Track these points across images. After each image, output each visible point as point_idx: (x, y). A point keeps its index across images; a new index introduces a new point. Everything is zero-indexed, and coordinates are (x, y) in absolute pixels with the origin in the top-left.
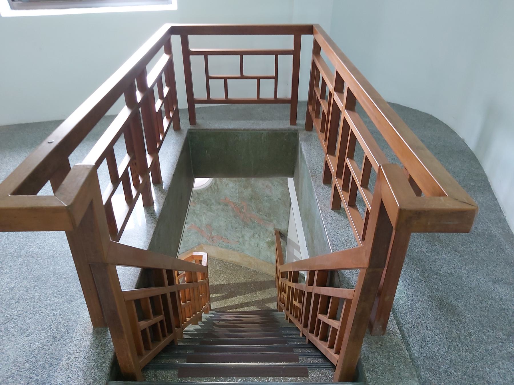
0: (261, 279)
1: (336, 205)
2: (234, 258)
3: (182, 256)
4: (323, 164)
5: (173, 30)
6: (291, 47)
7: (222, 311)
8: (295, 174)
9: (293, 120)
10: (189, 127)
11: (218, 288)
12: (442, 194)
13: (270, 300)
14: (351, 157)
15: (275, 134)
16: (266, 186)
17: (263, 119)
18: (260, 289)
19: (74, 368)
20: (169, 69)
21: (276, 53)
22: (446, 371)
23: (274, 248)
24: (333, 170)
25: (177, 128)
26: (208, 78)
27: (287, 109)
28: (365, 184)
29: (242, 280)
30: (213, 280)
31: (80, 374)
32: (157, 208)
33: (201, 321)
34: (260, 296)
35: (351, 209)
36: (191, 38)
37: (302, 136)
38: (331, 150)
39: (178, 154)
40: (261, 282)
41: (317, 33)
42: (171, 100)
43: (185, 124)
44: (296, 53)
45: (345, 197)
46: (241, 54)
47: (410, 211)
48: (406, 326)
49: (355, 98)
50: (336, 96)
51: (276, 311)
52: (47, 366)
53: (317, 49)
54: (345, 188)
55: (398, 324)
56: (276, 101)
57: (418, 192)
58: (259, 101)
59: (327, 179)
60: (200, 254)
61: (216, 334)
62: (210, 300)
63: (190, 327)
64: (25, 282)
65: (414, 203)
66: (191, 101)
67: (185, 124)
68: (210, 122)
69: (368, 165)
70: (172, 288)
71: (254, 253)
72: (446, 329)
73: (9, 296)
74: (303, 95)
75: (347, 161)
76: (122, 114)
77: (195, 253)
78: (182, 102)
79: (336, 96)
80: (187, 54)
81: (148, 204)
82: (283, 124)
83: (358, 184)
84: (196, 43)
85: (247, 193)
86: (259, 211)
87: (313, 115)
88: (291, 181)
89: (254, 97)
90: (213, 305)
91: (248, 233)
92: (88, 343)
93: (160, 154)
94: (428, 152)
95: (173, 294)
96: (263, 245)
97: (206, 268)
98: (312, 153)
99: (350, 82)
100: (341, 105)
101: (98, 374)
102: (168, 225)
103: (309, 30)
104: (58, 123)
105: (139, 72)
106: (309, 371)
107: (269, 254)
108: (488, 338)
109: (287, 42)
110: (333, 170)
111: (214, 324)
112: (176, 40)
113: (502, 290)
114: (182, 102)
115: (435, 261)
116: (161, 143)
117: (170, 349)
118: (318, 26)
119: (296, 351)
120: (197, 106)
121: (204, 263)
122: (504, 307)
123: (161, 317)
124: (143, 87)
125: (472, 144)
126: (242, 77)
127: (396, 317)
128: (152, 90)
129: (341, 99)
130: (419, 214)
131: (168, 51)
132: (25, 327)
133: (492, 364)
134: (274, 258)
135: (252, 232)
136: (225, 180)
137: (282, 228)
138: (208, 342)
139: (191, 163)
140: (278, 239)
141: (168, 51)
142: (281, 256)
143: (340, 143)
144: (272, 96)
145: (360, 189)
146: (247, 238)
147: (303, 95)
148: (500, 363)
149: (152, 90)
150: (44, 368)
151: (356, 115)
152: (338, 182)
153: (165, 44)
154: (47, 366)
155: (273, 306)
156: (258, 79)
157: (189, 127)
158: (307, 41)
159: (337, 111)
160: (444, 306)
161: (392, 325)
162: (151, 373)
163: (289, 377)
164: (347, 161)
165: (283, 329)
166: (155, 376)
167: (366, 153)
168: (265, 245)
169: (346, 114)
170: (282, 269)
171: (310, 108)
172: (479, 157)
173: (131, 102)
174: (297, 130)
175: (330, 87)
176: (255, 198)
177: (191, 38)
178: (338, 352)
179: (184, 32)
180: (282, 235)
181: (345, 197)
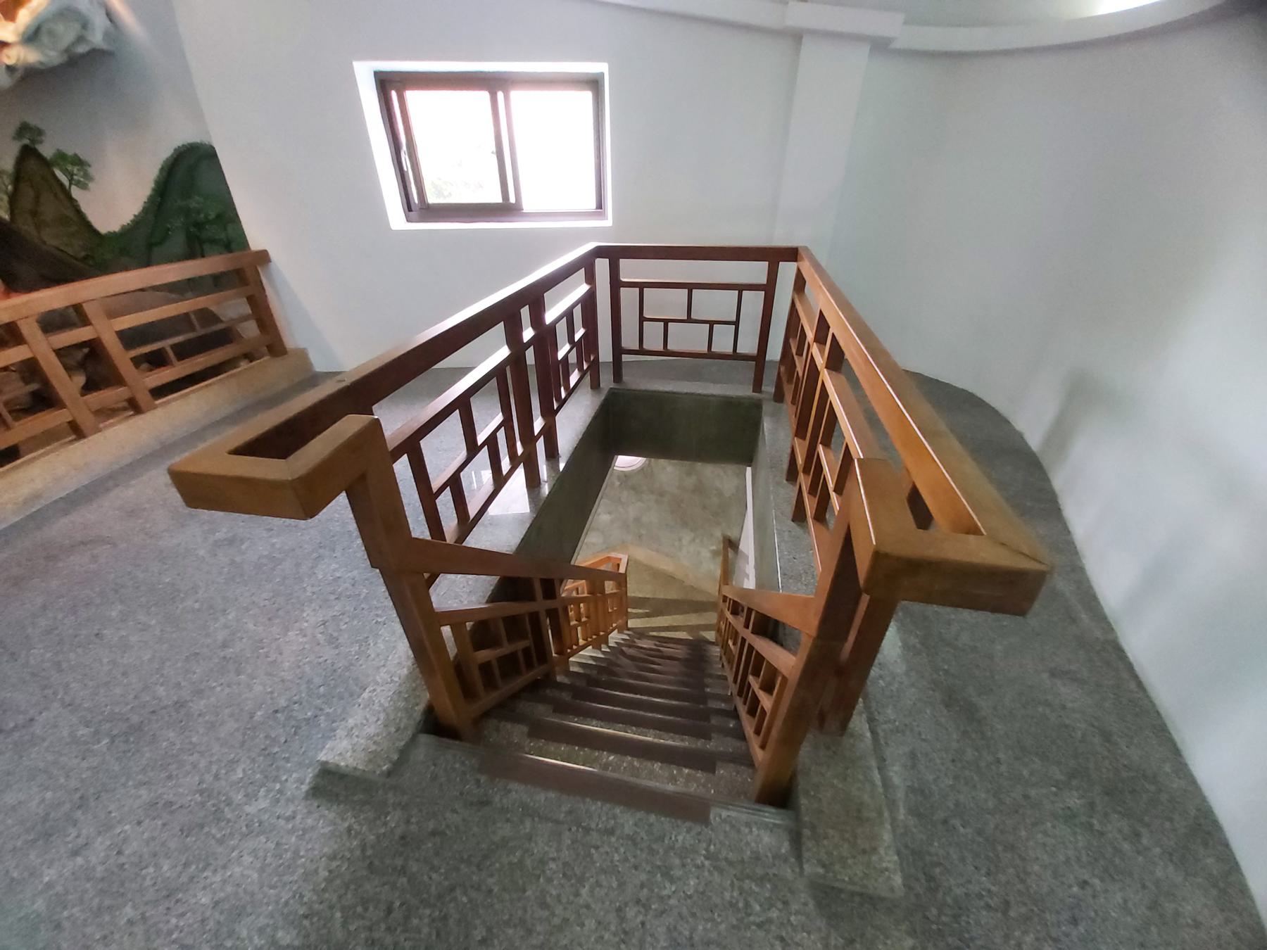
0: (699, 598)
1: (799, 515)
2: (665, 565)
3: (584, 557)
4: (789, 451)
5: (600, 252)
6: (764, 280)
7: (641, 633)
8: (83, 427)
9: (758, 385)
10: (612, 385)
11: (640, 602)
12: (974, 530)
13: (707, 628)
14: (827, 444)
15: (729, 404)
16: (718, 476)
17: (714, 382)
18: (696, 611)
19: (376, 707)
20: (588, 303)
21: (740, 288)
22: (945, 822)
23: (720, 559)
24: (800, 461)
25: (595, 385)
26: (642, 319)
27: (749, 369)
28: (839, 489)
29: (672, 594)
30: (634, 591)
31: (382, 716)
32: (546, 489)
33: (607, 643)
34: (693, 619)
35: (818, 524)
36: (624, 264)
37: (767, 407)
38: (800, 432)
39: (589, 420)
40: (697, 603)
41: (802, 259)
42: (588, 346)
43: (607, 380)
44: (769, 289)
45: (810, 505)
46: (690, 287)
47: (899, 559)
48: (885, 726)
49: (842, 353)
50: (815, 350)
51: (713, 643)
52: (346, 695)
53: (800, 284)
54: (812, 491)
55: (871, 720)
56: (735, 356)
57: (923, 517)
58: (710, 355)
59: (792, 475)
60: (619, 556)
61: (617, 669)
62: (627, 616)
63: (589, 652)
64: (355, 573)
65: (911, 542)
66: (618, 350)
67: (607, 380)
68: (639, 381)
69: (848, 456)
70: (550, 604)
71: (693, 562)
72: (955, 745)
73: (330, 589)
74: (774, 352)
75: (820, 449)
76: (491, 353)
77: (613, 555)
78: (605, 352)
79: (815, 350)
80: (616, 284)
81: (533, 481)
82: (741, 390)
83: (831, 486)
84: (631, 270)
85: (691, 481)
86: (704, 508)
87: (784, 379)
88: (749, 470)
89: (704, 349)
90: (631, 623)
91: (687, 537)
92: (405, 671)
93: (560, 418)
94: (956, 444)
95: (552, 613)
96: (706, 554)
97: (625, 576)
98: (777, 434)
99: (840, 327)
100: (820, 362)
101: (405, 721)
102: (562, 513)
103: (792, 254)
104: (469, 369)
105: (534, 297)
106: (719, 764)
107: (712, 567)
108: (1032, 774)
109: (756, 271)
110: (800, 461)
111: (623, 653)
112: (602, 266)
113: (1065, 691)
114: (605, 352)
115: (949, 623)
116: (562, 403)
117: (535, 689)
118: (806, 248)
119: (714, 721)
120: (625, 358)
121: (622, 570)
122: (1067, 722)
123: (521, 645)
124: (537, 320)
125: (1034, 440)
126: (689, 320)
127: (867, 707)
128: (552, 328)
129: (822, 352)
130: (915, 566)
131: (590, 278)
132: (335, 634)
133: (1034, 824)
134: (718, 572)
135: (693, 535)
136: (662, 462)
137: (732, 534)
138: (595, 687)
139: (607, 435)
140: (725, 549)
141: (590, 278)
142: (727, 574)
143: (816, 424)
144: (730, 350)
145: (833, 495)
146: (685, 542)
147: (774, 352)
148: (1049, 824)
149: (552, 328)
150: (342, 698)
151: (842, 377)
152: (804, 481)
153: (586, 264)
154: (346, 695)
155: (711, 635)
156: (712, 324)
157: (612, 385)
158: (787, 271)
159: (814, 372)
160: (956, 703)
161: (858, 722)
162: (493, 723)
163: (686, 767)
164: (820, 449)
165: (711, 676)
166: (497, 730)
167: (847, 440)
168: (708, 555)
169: (825, 376)
170: (727, 591)
171: (782, 369)
172: (1045, 462)
173: (513, 337)
174: (760, 400)
175: (810, 335)
176: (699, 489)
177: (624, 264)
178: (763, 747)
179: (614, 255)
180: (731, 545)
181: (810, 505)
